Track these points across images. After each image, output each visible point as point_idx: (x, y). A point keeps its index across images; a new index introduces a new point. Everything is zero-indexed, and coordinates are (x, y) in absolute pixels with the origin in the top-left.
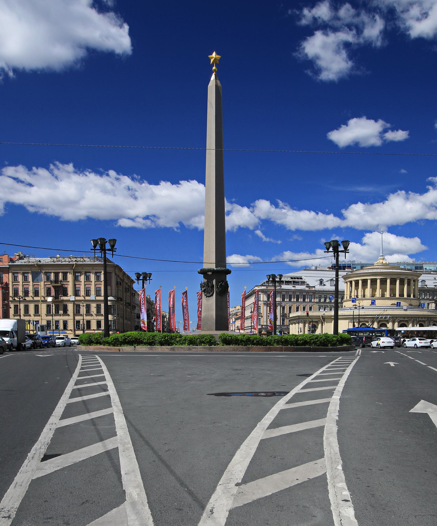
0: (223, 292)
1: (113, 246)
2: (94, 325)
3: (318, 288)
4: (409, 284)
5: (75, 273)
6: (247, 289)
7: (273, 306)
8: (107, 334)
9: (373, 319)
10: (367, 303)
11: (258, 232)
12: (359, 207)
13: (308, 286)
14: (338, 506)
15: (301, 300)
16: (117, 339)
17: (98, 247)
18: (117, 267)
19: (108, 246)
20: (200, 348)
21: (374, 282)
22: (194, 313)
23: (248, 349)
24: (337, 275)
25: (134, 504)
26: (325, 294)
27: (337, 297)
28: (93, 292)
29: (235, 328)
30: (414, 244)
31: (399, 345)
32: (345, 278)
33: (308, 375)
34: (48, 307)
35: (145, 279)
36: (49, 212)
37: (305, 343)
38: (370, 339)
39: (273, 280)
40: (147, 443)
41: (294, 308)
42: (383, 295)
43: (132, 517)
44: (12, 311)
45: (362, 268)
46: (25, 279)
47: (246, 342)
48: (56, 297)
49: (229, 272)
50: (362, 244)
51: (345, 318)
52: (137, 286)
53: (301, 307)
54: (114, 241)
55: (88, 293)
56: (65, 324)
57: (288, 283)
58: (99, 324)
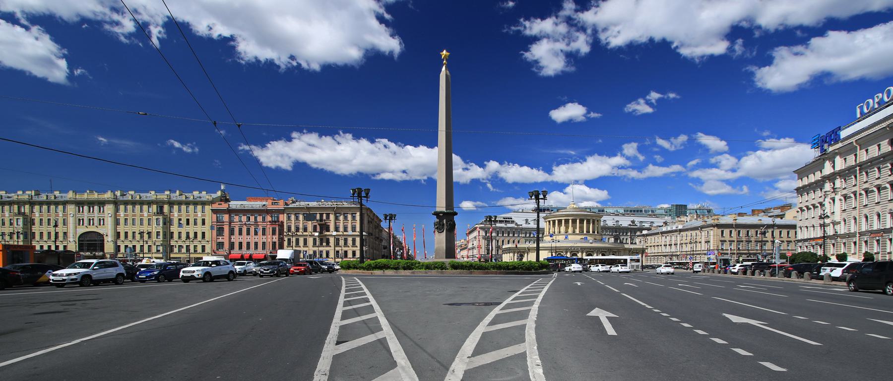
0: (451, 228)
1: (367, 194)
2: (350, 255)
3: (524, 226)
4: (593, 223)
5: (335, 214)
6: (469, 227)
7: (489, 239)
8: (362, 261)
9: (567, 249)
10: (561, 238)
11: (489, 185)
12: (563, 167)
13: (516, 224)
14: (532, 368)
15: (511, 235)
16: (370, 265)
17: (356, 195)
18: (369, 209)
19: (363, 194)
20: (434, 272)
21: (567, 221)
22: (428, 245)
23: (471, 273)
24: (538, 217)
25: (403, 368)
26: (529, 231)
27: (538, 233)
28: (349, 229)
29: (462, 256)
30: (603, 194)
31: (586, 270)
32: (545, 218)
33: (516, 292)
34: (315, 240)
35: (391, 219)
36: (329, 168)
37: (514, 268)
38: (564, 265)
39: (490, 220)
40: (405, 335)
41: (506, 241)
42: (574, 232)
43: (403, 375)
44: (286, 243)
45: (558, 211)
46: (297, 218)
47: (469, 267)
48: (321, 233)
49: (456, 214)
50: (565, 193)
51: (545, 249)
52: (384, 225)
53: (511, 241)
54: (369, 190)
55: (345, 230)
56: (328, 253)
57: (501, 222)
58: (354, 253)
